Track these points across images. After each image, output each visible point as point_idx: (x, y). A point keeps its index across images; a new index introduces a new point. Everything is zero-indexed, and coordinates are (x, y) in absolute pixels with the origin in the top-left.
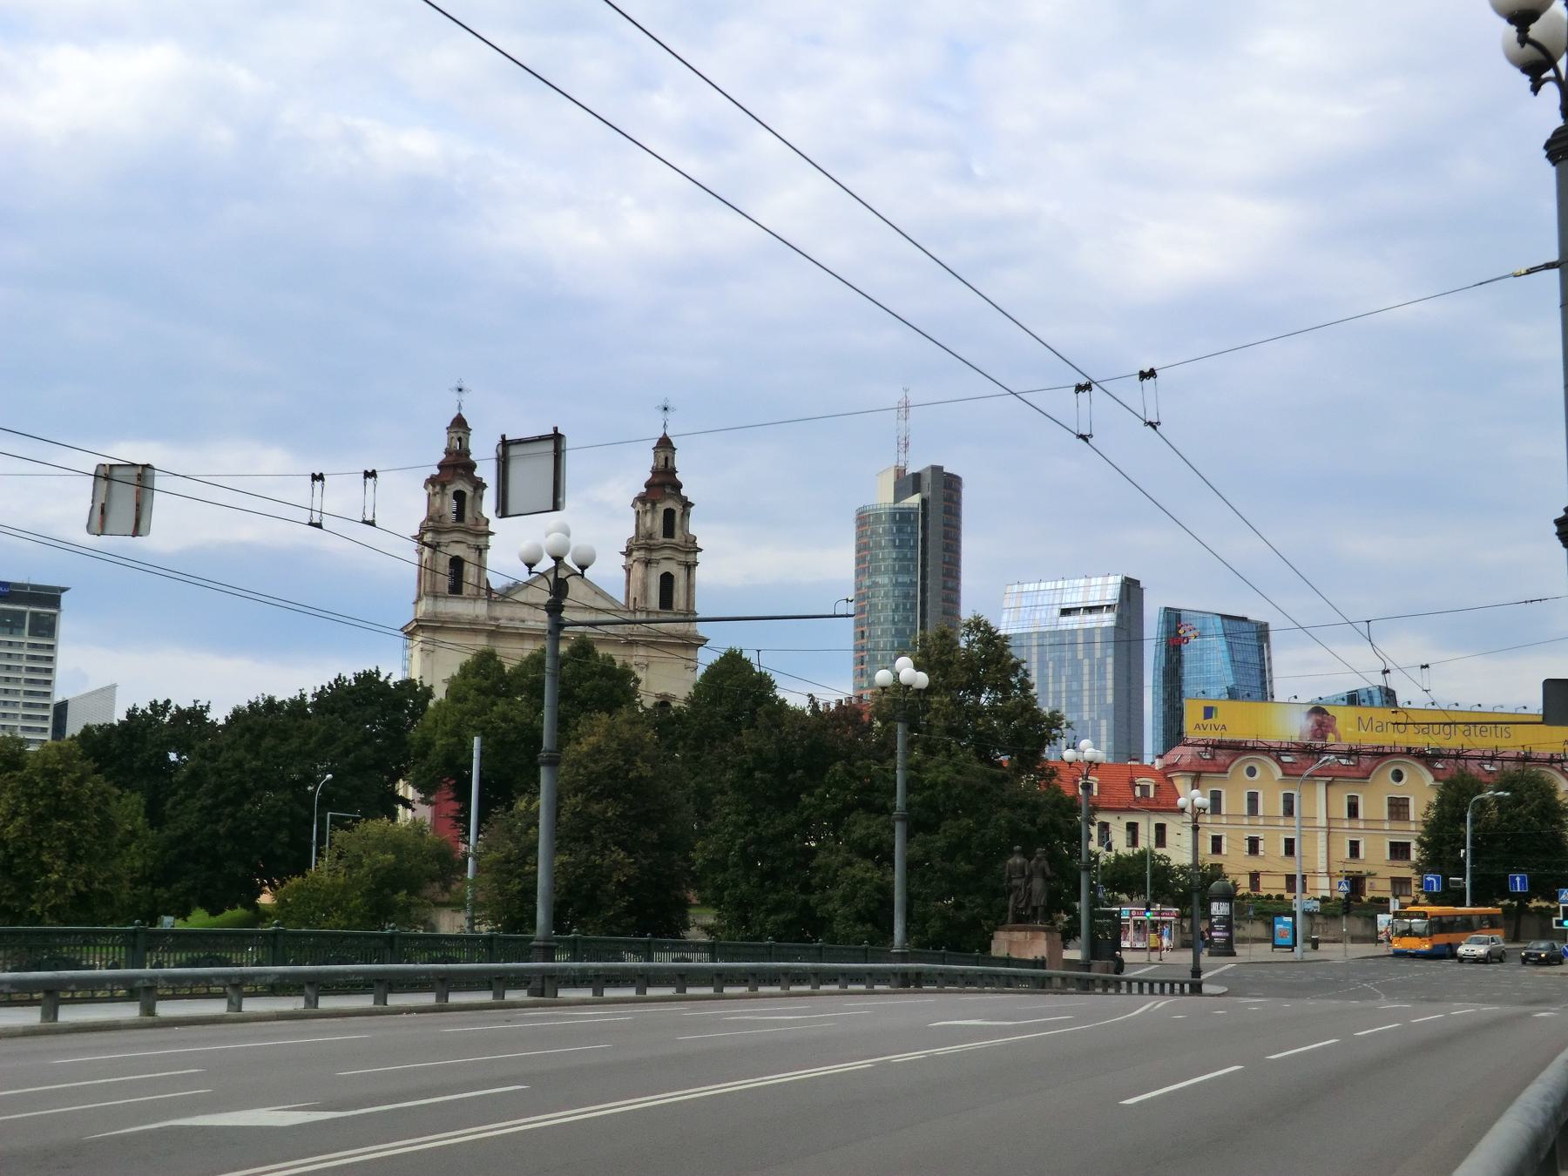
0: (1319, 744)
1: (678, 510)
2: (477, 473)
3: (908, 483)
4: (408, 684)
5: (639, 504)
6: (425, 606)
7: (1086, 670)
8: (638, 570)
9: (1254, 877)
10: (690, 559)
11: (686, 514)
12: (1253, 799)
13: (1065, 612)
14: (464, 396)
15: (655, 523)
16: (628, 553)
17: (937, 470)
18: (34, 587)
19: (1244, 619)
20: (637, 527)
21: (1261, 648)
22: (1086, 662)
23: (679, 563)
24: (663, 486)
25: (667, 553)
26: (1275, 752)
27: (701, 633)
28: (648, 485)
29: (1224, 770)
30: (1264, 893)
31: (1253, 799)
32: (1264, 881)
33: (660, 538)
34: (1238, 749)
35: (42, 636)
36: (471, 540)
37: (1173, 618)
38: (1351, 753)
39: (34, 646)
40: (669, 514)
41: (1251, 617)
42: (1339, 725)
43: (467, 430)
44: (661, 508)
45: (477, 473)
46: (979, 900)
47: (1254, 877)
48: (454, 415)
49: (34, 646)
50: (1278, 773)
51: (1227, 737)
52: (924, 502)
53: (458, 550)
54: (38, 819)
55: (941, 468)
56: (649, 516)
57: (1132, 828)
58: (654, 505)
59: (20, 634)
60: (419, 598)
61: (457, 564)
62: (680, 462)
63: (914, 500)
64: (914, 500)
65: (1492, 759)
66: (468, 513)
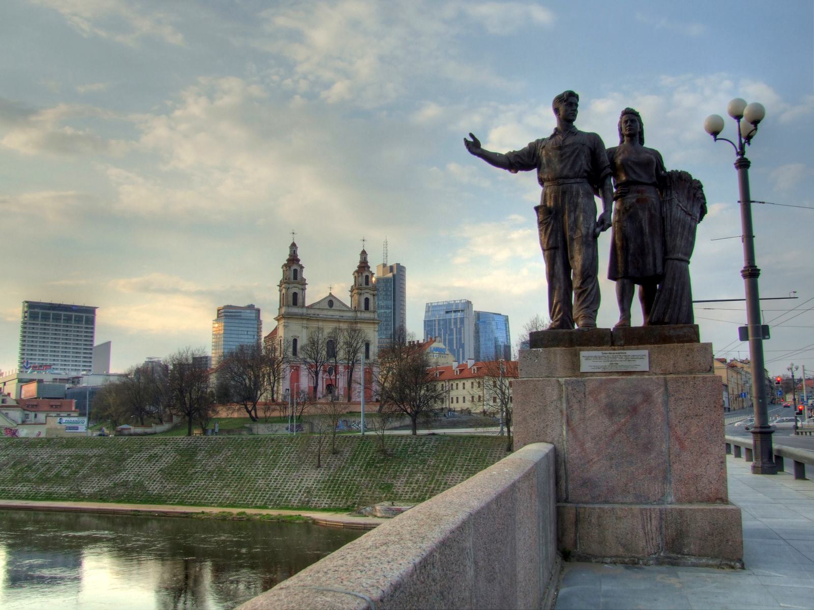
2: (300, 263)
5: (356, 274)
6: (283, 310)
7: (455, 332)
8: (356, 297)
10: (303, 287)
14: (295, 236)
15: (362, 280)
16: (352, 291)
17: (398, 265)
18: (86, 307)
19: (500, 314)
20: (355, 282)
21: (506, 324)
22: (455, 329)
23: (371, 294)
24: (293, 259)
25: (367, 291)
33: (364, 285)
35: (89, 324)
36: (300, 287)
39: (87, 328)
40: (295, 271)
41: (502, 314)
43: (297, 248)
44: (364, 275)
45: (300, 263)
46: (317, 421)
48: (292, 242)
49: (87, 328)
52: (394, 276)
53: (296, 290)
54: (537, 412)
55: (399, 264)
56: (360, 278)
58: (362, 274)
59: (81, 324)
60: (280, 307)
61: (295, 295)
62: (369, 259)
64: (390, 275)
66: (299, 277)
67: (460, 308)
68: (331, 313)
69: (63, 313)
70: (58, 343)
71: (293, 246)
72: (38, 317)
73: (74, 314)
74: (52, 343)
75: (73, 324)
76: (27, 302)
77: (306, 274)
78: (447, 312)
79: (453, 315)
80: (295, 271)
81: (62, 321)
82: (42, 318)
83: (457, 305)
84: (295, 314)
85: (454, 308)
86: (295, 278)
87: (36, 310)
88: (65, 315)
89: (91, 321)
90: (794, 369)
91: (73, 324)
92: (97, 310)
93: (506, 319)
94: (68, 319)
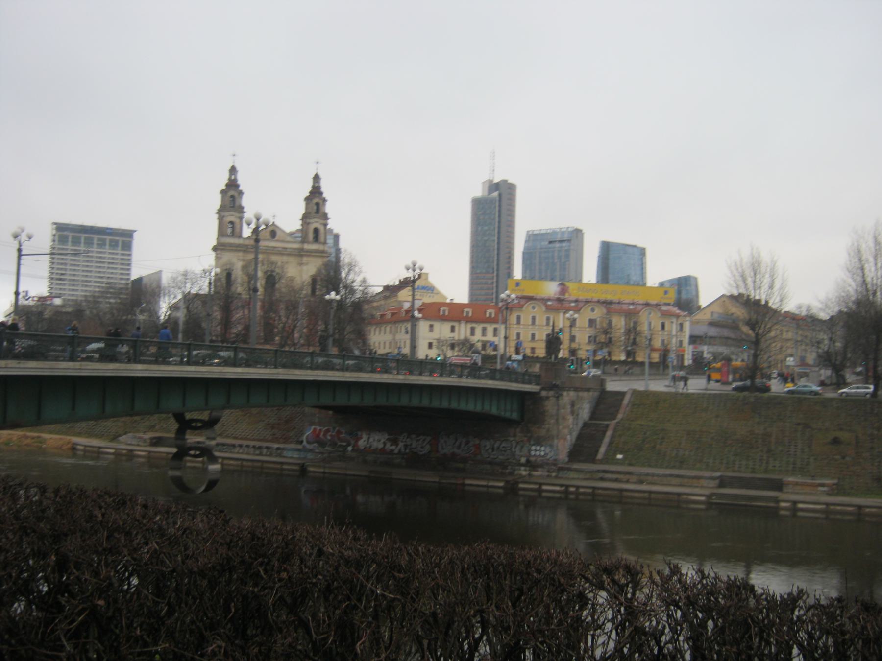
0: (562, 297)
1: (321, 202)
3: (494, 187)
4: (740, 294)
9: (533, 349)
11: (324, 205)
12: (534, 318)
13: (550, 242)
19: (634, 246)
26: (544, 300)
27: (871, 244)
28: (311, 193)
29: (522, 307)
30: (535, 355)
31: (534, 318)
32: (537, 351)
34: (530, 298)
37: (607, 249)
38: (576, 301)
39: (123, 254)
42: (571, 290)
47: (533, 349)
49: (123, 254)
50: (544, 308)
51: (525, 294)
52: (500, 195)
57: (484, 330)
59: (79, 246)
63: (496, 194)
64: (496, 194)
65: (633, 304)
66: (321, 211)
67: (566, 237)
68: (273, 244)
69: (96, 237)
70: (91, 271)
71: (317, 178)
72: (80, 243)
73: (108, 238)
74: (83, 271)
75: (107, 249)
76: (55, 224)
77: (329, 209)
78: (550, 242)
79: (557, 245)
80: (317, 204)
81: (95, 246)
82: (72, 242)
83: (563, 233)
84: (231, 245)
85: (559, 238)
86: (318, 211)
87: (65, 233)
88: (99, 239)
89: (127, 246)
90: (23, 237)
91: (107, 249)
92: (135, 234)
93: (642, 252)
94: (102, 244)
